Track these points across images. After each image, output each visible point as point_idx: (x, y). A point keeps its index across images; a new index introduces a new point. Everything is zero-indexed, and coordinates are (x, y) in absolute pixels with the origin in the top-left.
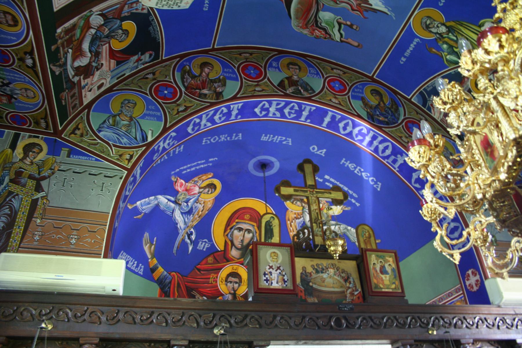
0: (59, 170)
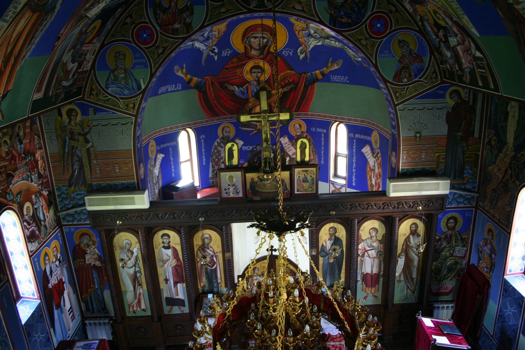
0: (93, 126)
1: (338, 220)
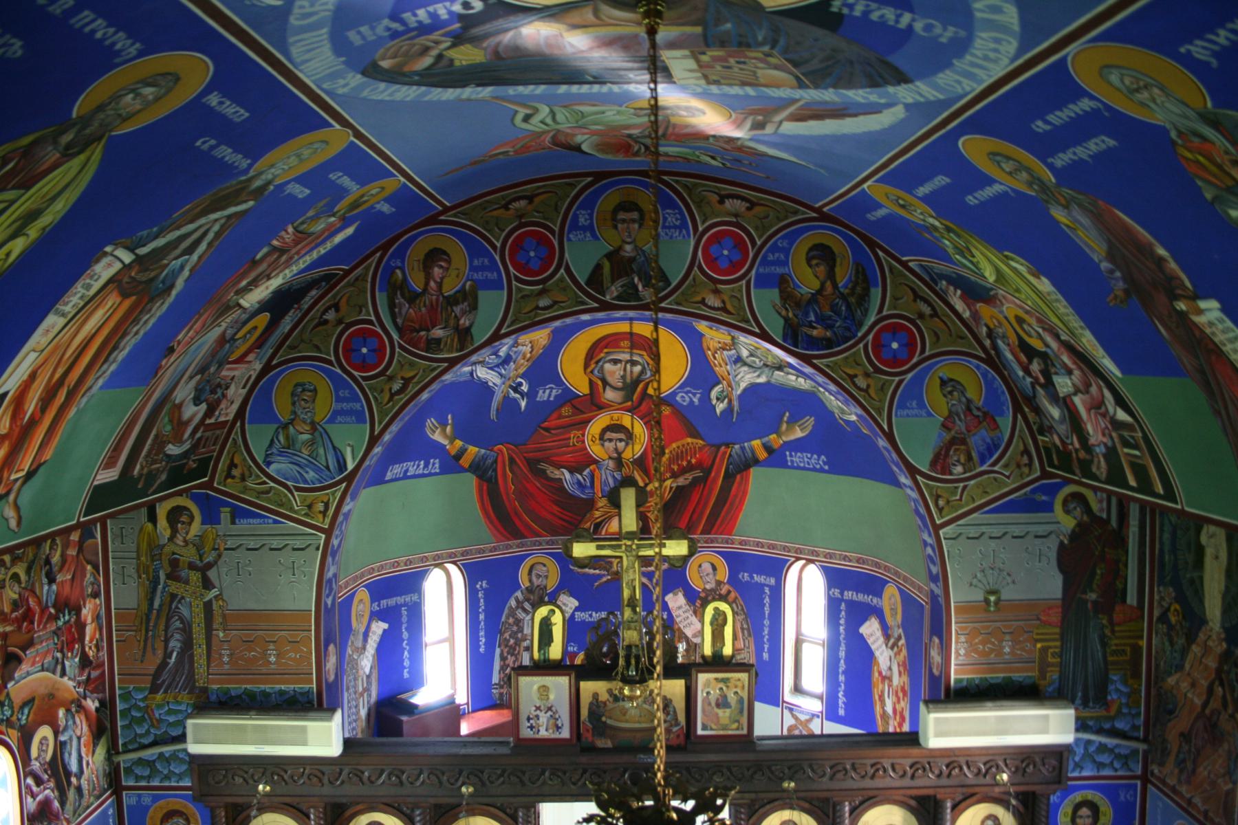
1: (803, 804)
